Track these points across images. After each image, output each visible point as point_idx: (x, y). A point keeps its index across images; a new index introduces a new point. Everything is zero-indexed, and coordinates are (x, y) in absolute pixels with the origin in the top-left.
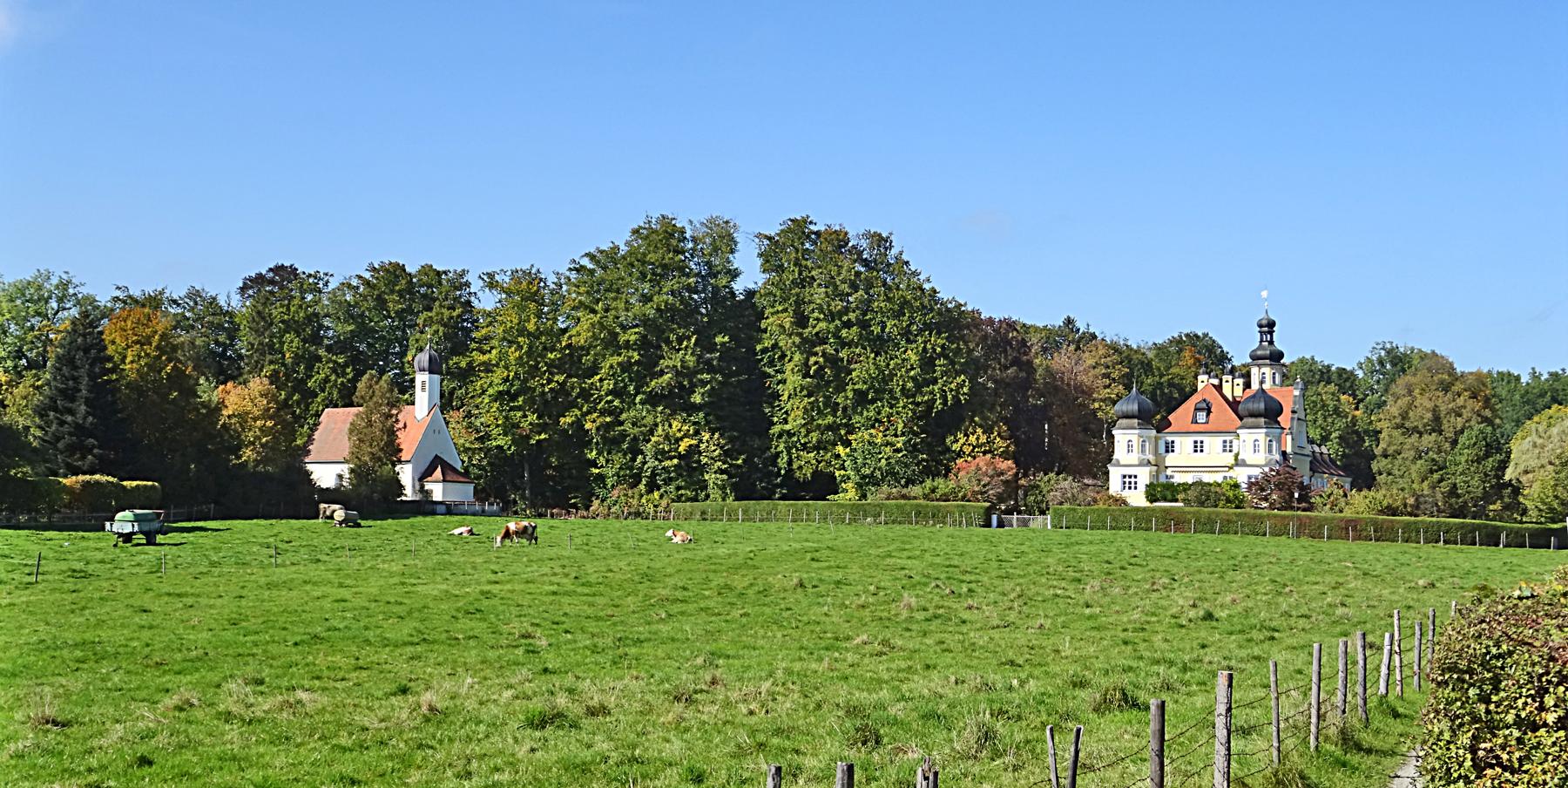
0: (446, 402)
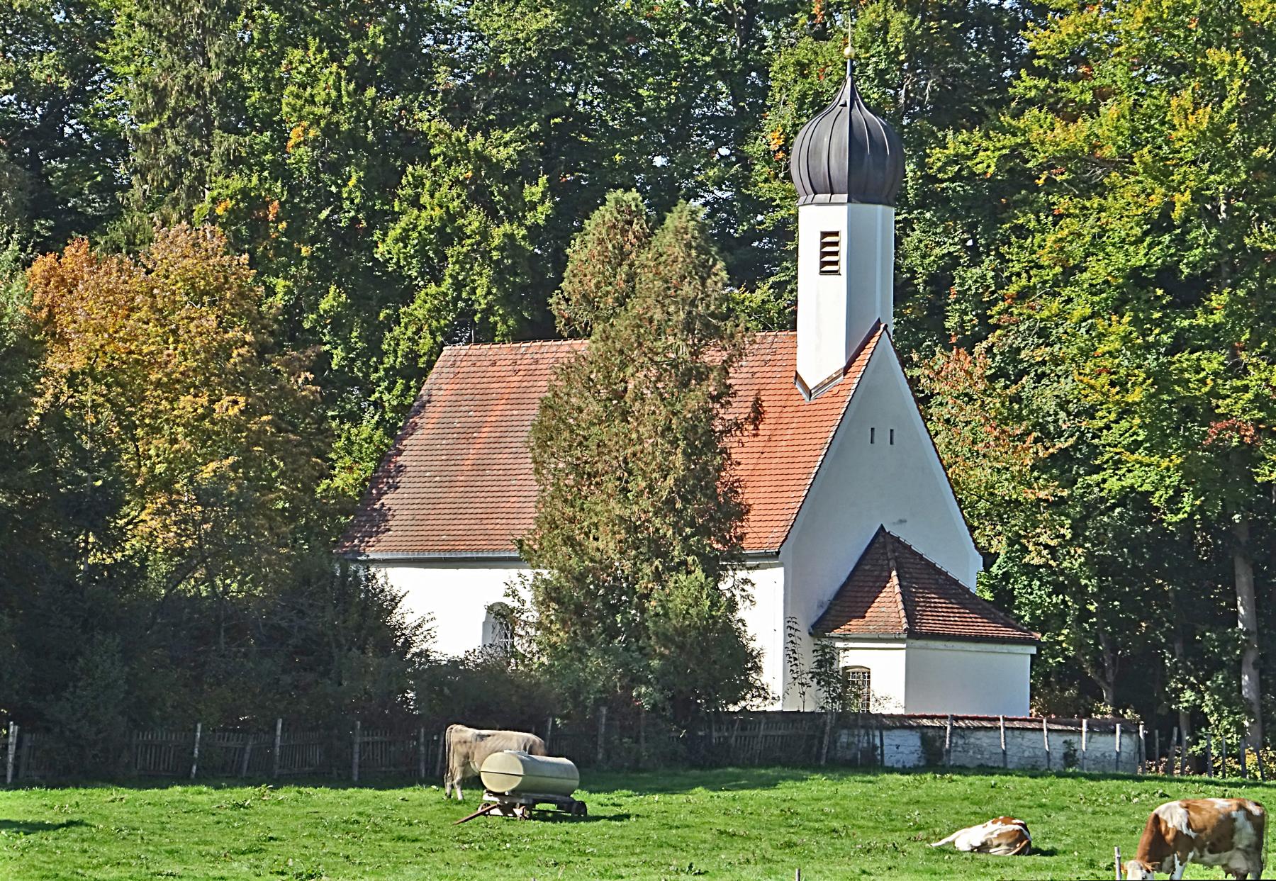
0: (918, 316)
